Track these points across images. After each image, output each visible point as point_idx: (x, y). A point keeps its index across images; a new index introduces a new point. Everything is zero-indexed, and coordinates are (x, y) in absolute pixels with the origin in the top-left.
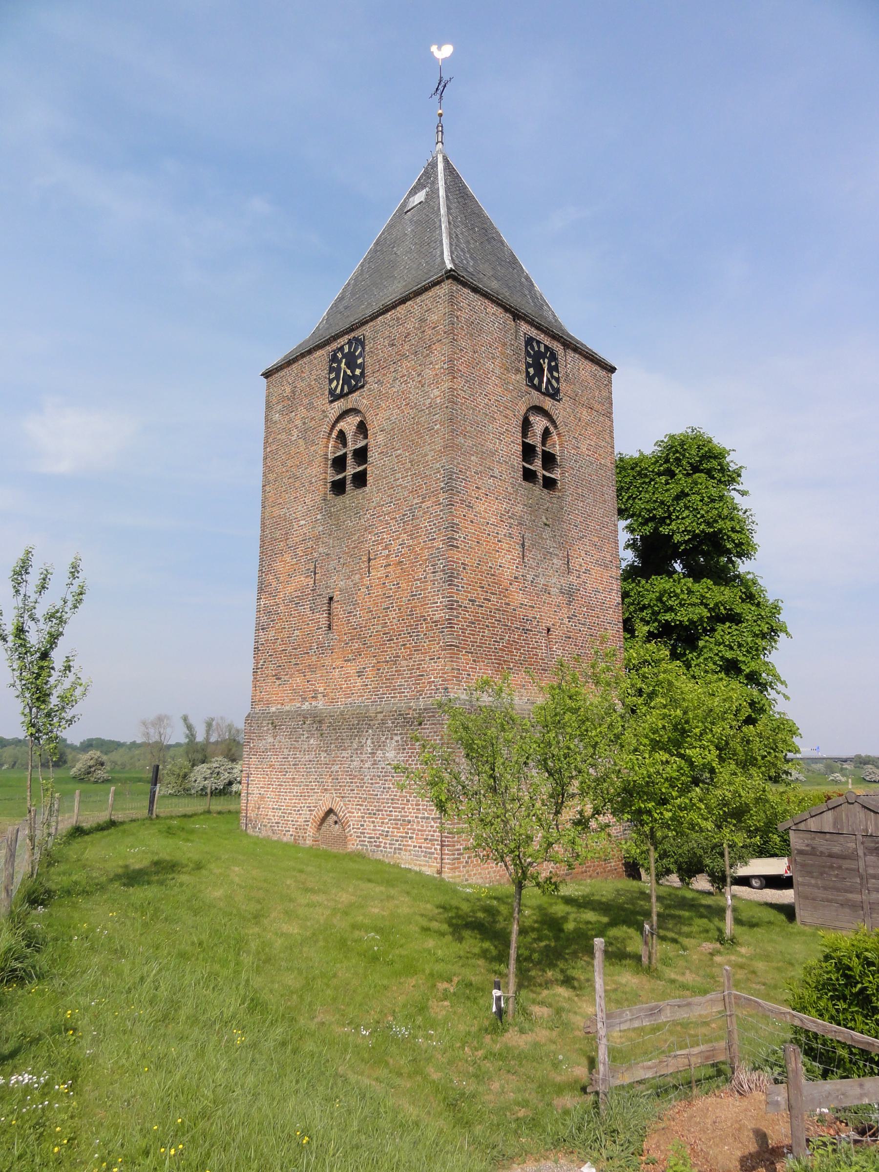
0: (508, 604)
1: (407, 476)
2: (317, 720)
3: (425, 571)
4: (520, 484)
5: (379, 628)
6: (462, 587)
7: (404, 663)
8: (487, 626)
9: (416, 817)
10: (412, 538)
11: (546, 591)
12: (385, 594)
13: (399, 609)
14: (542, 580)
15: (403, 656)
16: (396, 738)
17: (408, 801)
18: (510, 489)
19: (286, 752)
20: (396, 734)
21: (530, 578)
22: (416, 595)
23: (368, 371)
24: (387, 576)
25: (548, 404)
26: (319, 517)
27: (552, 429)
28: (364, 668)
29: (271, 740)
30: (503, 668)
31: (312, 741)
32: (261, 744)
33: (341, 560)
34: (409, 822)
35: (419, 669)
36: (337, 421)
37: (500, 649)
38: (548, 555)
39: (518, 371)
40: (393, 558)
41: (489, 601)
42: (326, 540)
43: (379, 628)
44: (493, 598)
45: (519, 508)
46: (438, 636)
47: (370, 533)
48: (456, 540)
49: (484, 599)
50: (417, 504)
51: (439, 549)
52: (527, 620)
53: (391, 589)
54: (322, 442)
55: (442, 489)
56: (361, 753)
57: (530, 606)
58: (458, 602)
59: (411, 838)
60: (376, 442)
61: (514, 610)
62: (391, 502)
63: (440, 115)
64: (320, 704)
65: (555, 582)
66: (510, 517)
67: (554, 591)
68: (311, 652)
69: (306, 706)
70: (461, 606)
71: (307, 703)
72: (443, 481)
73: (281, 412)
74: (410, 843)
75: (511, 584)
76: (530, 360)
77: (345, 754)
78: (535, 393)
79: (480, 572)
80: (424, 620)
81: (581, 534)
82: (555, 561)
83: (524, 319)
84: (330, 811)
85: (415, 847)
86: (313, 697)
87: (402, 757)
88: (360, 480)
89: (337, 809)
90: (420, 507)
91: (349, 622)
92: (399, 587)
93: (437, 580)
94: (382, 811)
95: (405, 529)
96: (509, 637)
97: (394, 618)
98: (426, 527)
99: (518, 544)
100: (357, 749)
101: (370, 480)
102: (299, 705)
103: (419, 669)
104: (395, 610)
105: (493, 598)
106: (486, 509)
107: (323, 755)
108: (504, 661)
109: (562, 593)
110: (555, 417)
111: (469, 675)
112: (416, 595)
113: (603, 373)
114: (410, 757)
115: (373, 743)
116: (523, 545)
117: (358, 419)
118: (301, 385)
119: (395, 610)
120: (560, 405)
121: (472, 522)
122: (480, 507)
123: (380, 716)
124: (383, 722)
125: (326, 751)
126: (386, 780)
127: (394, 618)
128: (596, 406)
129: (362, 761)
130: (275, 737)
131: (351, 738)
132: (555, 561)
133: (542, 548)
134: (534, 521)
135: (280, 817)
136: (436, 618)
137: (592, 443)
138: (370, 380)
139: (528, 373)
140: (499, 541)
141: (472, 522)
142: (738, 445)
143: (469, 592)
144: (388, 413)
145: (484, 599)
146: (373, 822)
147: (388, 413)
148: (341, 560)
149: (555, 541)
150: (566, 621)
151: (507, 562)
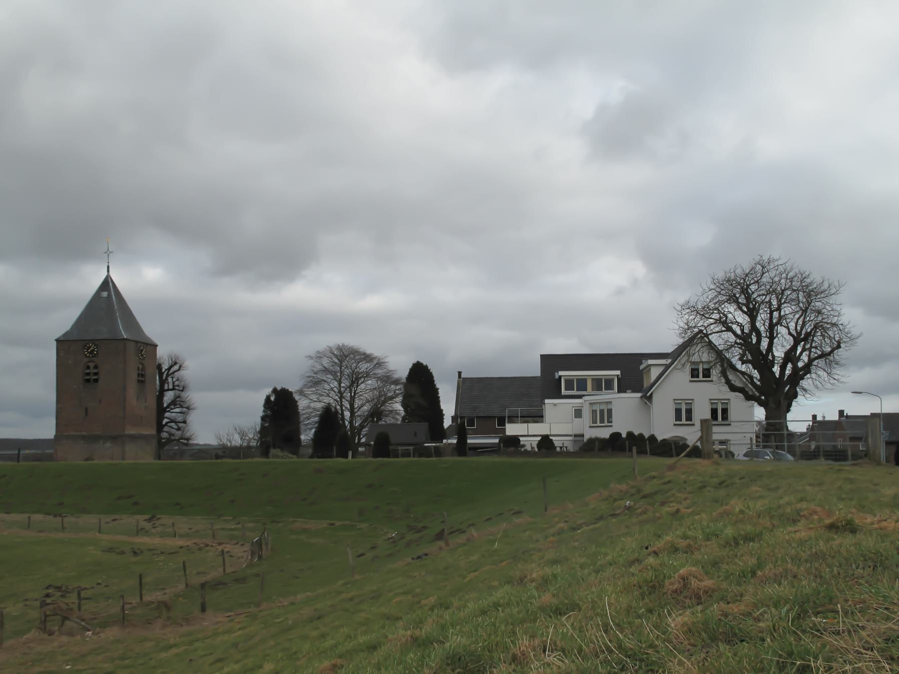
88: (96, 381)
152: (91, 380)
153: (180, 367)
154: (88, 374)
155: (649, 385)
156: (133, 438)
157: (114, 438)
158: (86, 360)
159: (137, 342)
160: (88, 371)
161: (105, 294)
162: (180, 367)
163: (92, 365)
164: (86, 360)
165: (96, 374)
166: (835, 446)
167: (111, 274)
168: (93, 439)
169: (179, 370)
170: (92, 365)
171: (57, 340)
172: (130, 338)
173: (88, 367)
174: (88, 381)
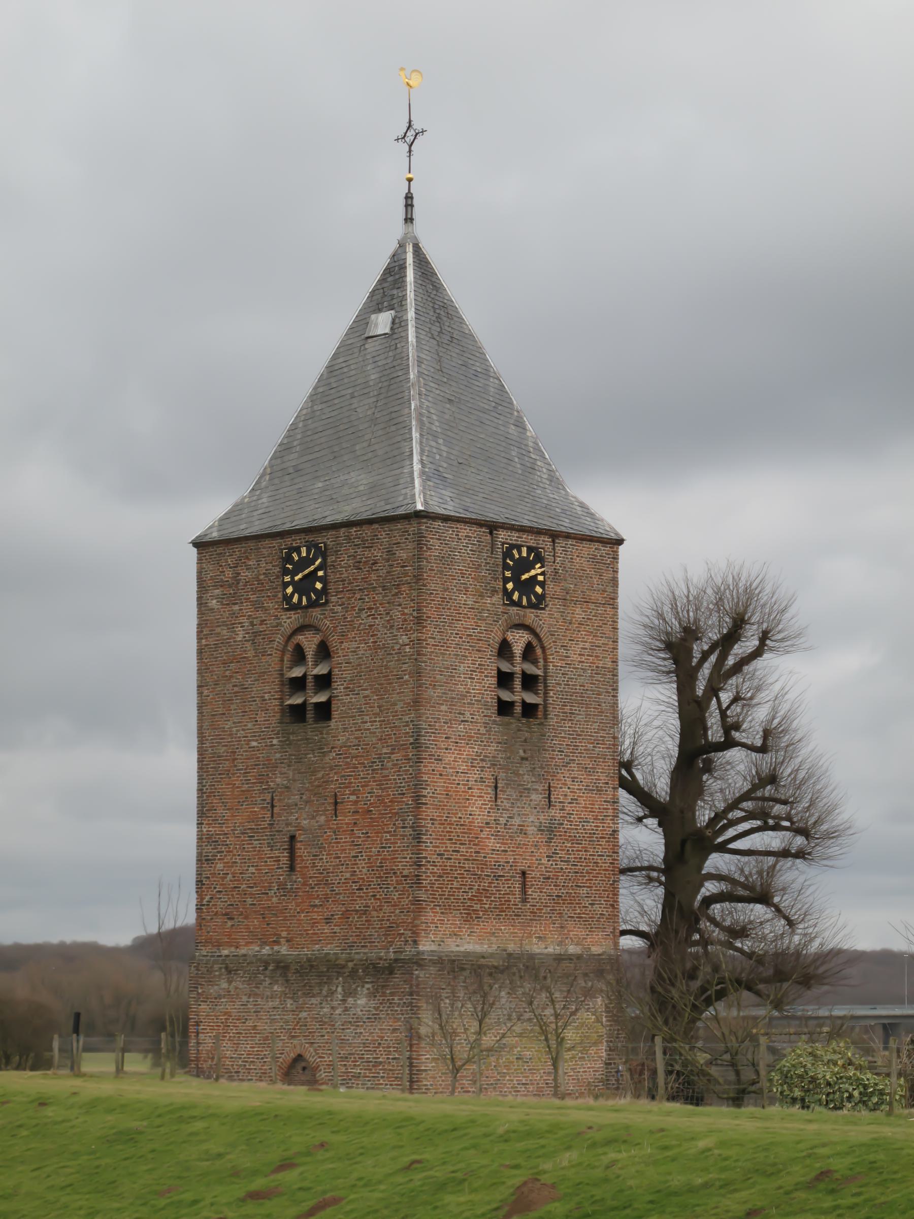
0: (478, 852)
1: (375, 721)
2: (282, 967)
3: (394, 824)
4: (494, 721)
5: (348, 875)
6: (431, 843)
7: (374, 913)
8: (456, 878)
9: (388, 1058)
10: (381, 789)
11: (522, 831)
12: (353, 841)
13: (369, 859)
14: (517, 821)
15: (374, 907)
16: (367, 986)
17: (379, 1044)
18: (483, 730)
19: (245, 999)
20: (367, 983)
21: (502, 821)
22: (385, 847)
23: (332, 587)
24: (355, 823)
25: (530, 617)
26: (275, 742)
27: (535, 643)
28: (332, 915)
29: (225, 985)
30: (471, 918)
31: (276, 988)
32: (213, 990)
33: (304, 797)
34: (381, 1063)
35: (388, 920)
36: (296, 632)
37: (469, 899)
38: (525, 791)
39: (494, 591)
40: (361, 805)
41: (458, 851)
42: (284, 770)
43: (348, 875)
44: (463, 849)
45: (493, 747)
46: (408, 891)
47: (336, 773)
48: (425, 796)
49: (453, 851)
50: (386, 753)
51: (407, 804)
52: (499, 866)
53: (360, 837)
54: (276, 656)
55: (411, 744)
56: (331, 1000)
57: (503, 851)
58: (426, 858)
59: (382, 1077)
60: (343, 667)
61: (485, 857)
62: (359, 745)
63: (410, 180)
64: (284, 950)
65: (533, 819)
66: (482, 760)
67: (531, 830)
68: (271, 893)
69: (266, 950)
70: (429, 862)
71: (267, 948)
72: (413, 736)
73: (220, 599)
74: (381, 1082)
75: (481, 831)
76: (508, 574)
77: (314, 1001)
78: (514, 610)
79: (448, 824)
80: (395, 873)
81: (567, 760)
82: (534, 797)
83: (502, 528)
84: (299, 1058)
85: (386, 1085)
86: (274, 941)
87: (373, 1003)
88: (324, 711)
89: (307, 1056)
90: (390, 758)
91: (314, 865)
92: (369, 837)
93: (406, 836)
94: (353, 1054)
95: (374, 777)
96: (479, 886)
97: (363, 867)
98: (395, 779)
99: (489, 786)
100: (326, 996)
101: (335, 714)
102: (257, 948)
103: (388, 920)
104: (364, 860)
105: (463, 849)
106: (455, 758)
107: (289, 1002)
108: (474, 910)
109: (539, 830)
110: (538, 630)
111: (437, 927)
112: (385, 847)
113: (605, 550)
114: (381, 1003)
115: (344, 990)
116: (496, 787)
117: (317, 639)
118: (245, 575)
119: (364, 860)
120: (544, 614)
121: (441, 775)
122: (449, 758)
123: (350, 965)
124: (354, 972)
125: (292, 998)
126: (358, 1026)
127: (363, 867)
128: (595, 596)
129: (332, 1008)
130: (230, 982)
131: (320, 984)
132: (534, 797)
133: (519, 785)
134: (509, 758)
135: (241, 1065)
136: (406, 872)
137: (587, 645)
138: (333, 599)
139: (505, 589)
140: (469, 788)
141: (441, 775)
142: (808, 594)
143: (438, 847)
144: (354, 645)
145: (453, 851)
146: (345, 1065)
147: (354, 645)
148: (304, 797)
149: (533, 775)
150: (544, 861)
151: (478, 809)
152: (307, 709)
153: (765, 637)
154: (298, 684)
155: (371, 334)
156: (478, 976)
157: (388, 973)
158: (290, 620)
159: (492, 527)
160: (297, 672)
161: (382, 322)
162: (765, 637)
163: (309, 642)
164: (290, 620)
165: (324, 682)
166: (324, 1200)
167: (422, 230)
168: (308, 975)
169: (757, 653)
170: (309, 642)
171: (200, 545)
172: (450, 508)
173: (299, 656)
174: (298, 713)
